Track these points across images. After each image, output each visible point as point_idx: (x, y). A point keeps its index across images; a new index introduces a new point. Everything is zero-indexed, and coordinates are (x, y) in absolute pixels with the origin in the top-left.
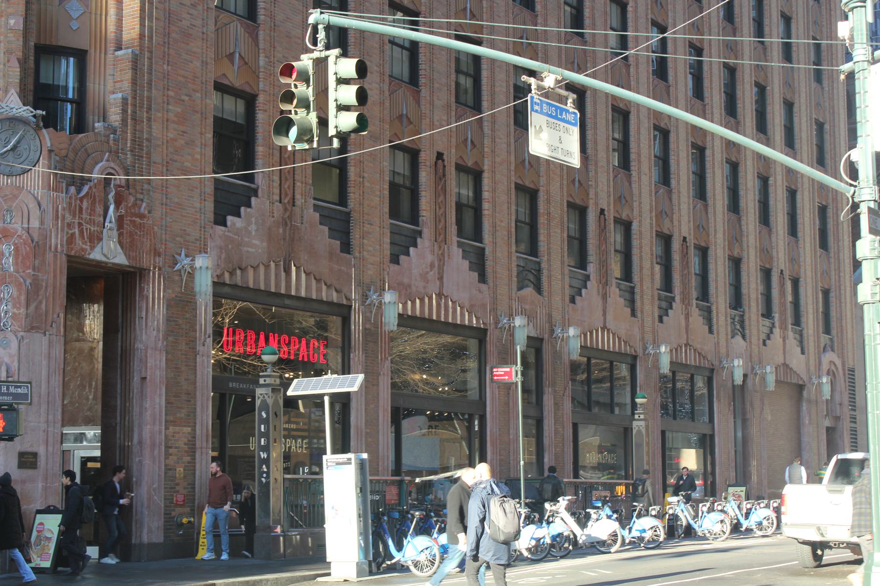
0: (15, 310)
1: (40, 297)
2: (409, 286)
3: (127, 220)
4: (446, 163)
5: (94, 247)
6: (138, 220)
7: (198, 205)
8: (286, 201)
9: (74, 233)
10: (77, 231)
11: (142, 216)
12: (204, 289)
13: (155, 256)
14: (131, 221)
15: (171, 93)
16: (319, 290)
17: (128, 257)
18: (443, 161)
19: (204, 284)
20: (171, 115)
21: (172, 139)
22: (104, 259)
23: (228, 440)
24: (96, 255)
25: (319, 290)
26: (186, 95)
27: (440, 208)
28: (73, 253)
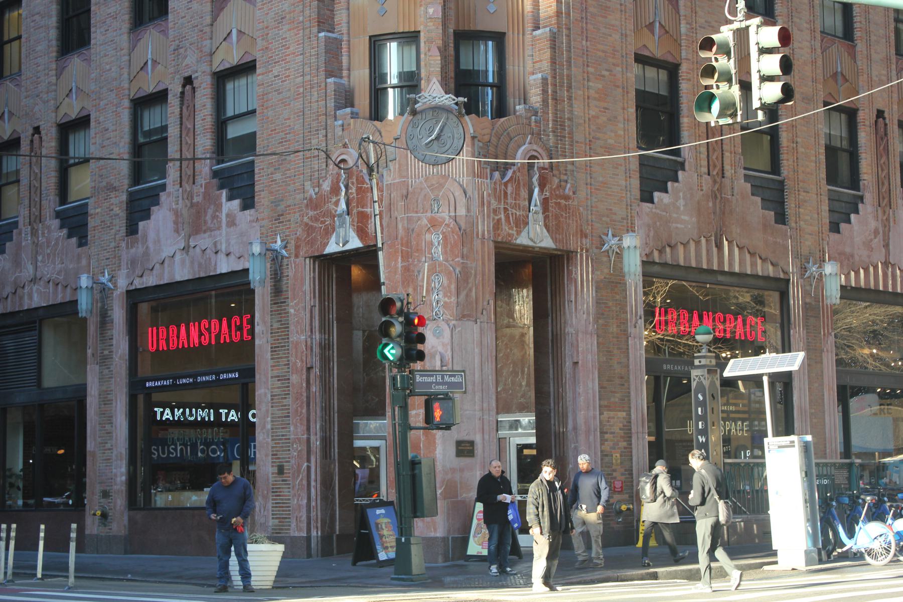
0: (446, 299)
1: (470, 285)
2: (852, 256)
3: (552, 203)
4: (887, 121)
5: (521, 232)
6: (563, 202)
7: (624, 183)
8: (715, 173)
9: (500, 219)
10: (502, 216)
11: (567, 198)
12: (632, 270)
13: (581, 238)
14: (556, 203)
15: (591, 70)
16: (753, 265)
17: (555, 240)
18: (884, 119)
19: (633, 264)
20: (592, 92)
21: (594, 117)
22: (531, 244)
23: (665, 424)
24: (523, 240)
25: (753, 265)
26: (606, 70)
27: (882, 170)
28: (500, 239)
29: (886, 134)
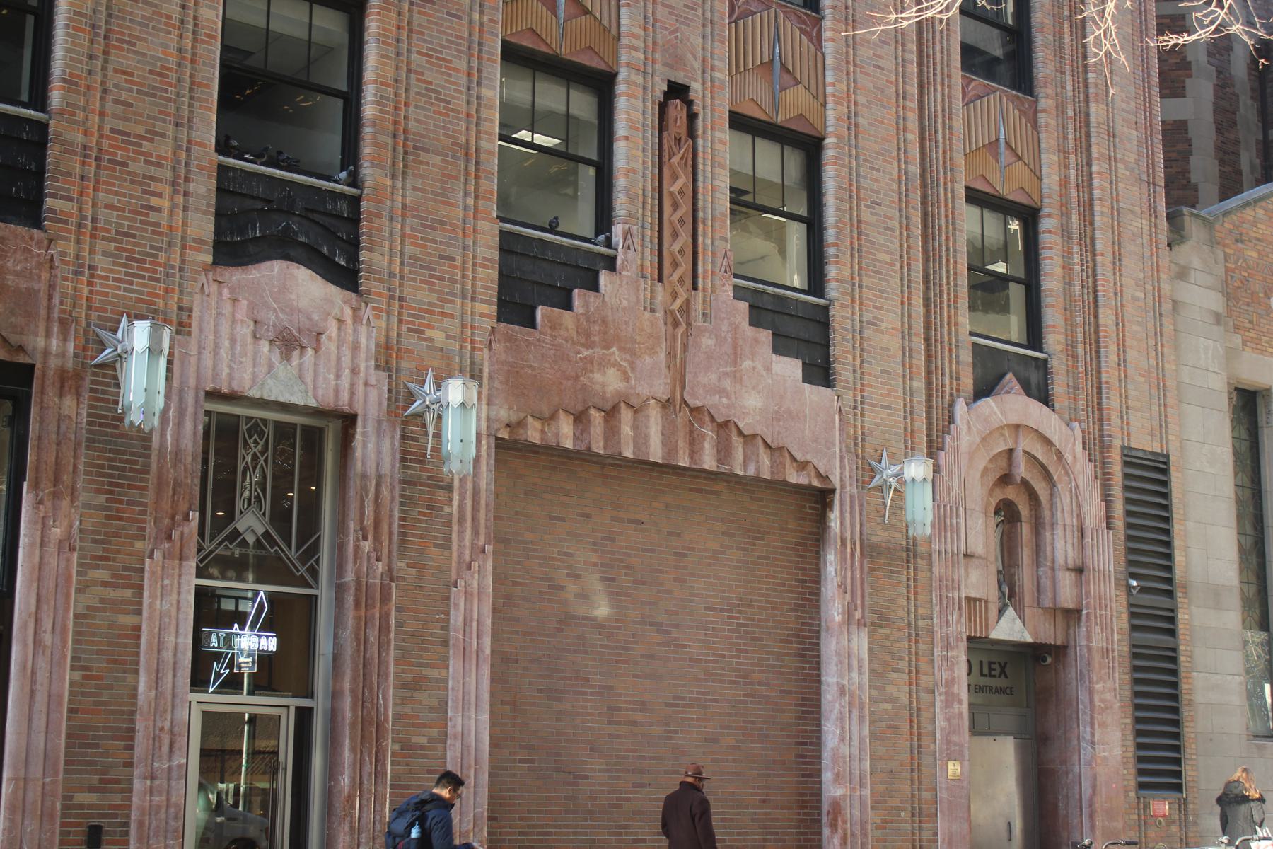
12: (918, 518)
27: (675, 206)
29: (692, 134)
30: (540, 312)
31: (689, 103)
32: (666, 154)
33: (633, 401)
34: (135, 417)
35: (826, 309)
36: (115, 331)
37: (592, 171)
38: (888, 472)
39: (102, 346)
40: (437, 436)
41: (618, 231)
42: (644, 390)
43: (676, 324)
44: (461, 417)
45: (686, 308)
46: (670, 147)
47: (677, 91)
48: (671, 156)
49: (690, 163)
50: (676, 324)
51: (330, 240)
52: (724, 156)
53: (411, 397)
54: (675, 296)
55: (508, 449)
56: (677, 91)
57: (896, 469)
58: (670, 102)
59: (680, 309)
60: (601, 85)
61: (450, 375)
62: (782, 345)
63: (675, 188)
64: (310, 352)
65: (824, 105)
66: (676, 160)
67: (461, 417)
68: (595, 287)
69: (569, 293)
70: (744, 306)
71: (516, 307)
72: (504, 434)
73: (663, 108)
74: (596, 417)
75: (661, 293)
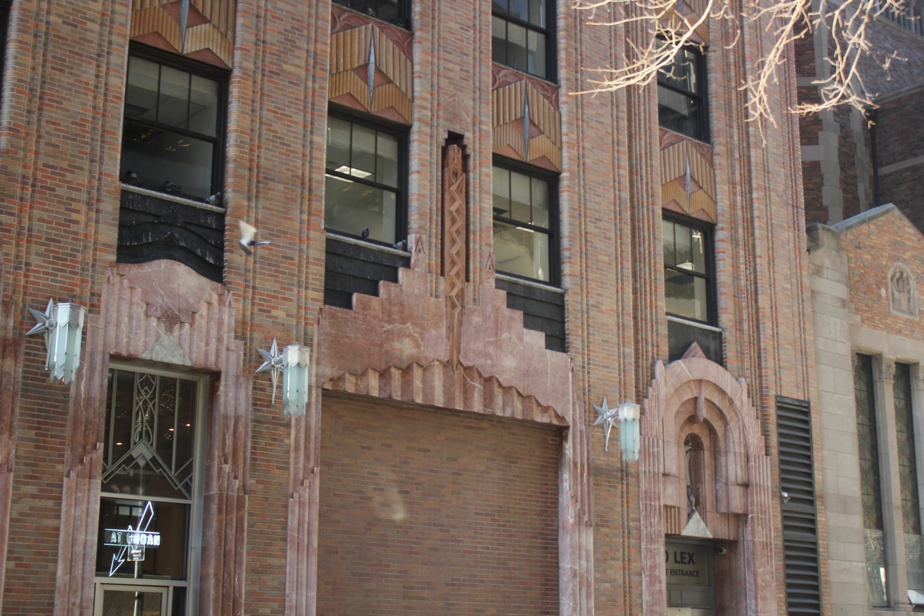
12: (630, 447)
27: (453, 221)
29: (465, 169)
30: (355, 297)
31: (463, 148)
32: (447, 184)
33: (423, 362)
34: (58, 374)
35: (562, 296)
36: (44, 310)
37: (393, 196)
38: (608, 414)
39: (34, 321)
40: (280, 387)
41: (412, 239)
42: (430, 354)
43: (454, 306)
44: (296, 373)
45: (461, 295)
46: (449, 178)
47: (455, 138)
48: (451, 184)
49: (464, 190)
50: (454, 306)
51: (205, 248)
52: (488, 185)
53: (261, 359)
54: (453, 286)
55: (331, 397)
56: (455, 138)
57: (613, 411)
58: (450, 147)
59: (457, 295)
60: (400, 134)
61: (289, 343)
62: (531, 322)
63: (453, 208)
64: (187, 326)
65: (561, 149)
66: (454, 188)
67: (296, 373)
68: (395, 279)
69: (376, 284)
70: (503, 293)
71: (337, 293)
72: (328, 386)
73: (445, 151)
74: (396, 373)
75: (443, 284)
